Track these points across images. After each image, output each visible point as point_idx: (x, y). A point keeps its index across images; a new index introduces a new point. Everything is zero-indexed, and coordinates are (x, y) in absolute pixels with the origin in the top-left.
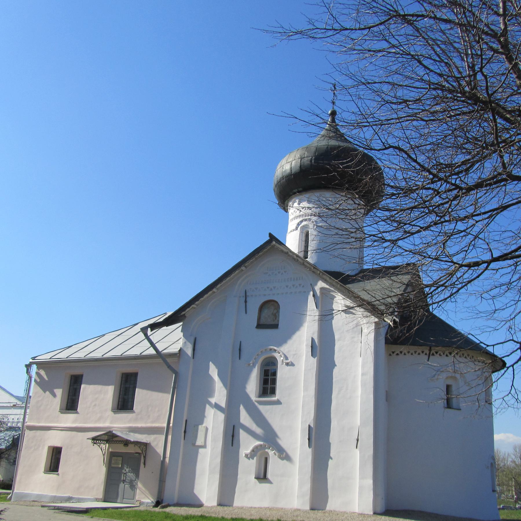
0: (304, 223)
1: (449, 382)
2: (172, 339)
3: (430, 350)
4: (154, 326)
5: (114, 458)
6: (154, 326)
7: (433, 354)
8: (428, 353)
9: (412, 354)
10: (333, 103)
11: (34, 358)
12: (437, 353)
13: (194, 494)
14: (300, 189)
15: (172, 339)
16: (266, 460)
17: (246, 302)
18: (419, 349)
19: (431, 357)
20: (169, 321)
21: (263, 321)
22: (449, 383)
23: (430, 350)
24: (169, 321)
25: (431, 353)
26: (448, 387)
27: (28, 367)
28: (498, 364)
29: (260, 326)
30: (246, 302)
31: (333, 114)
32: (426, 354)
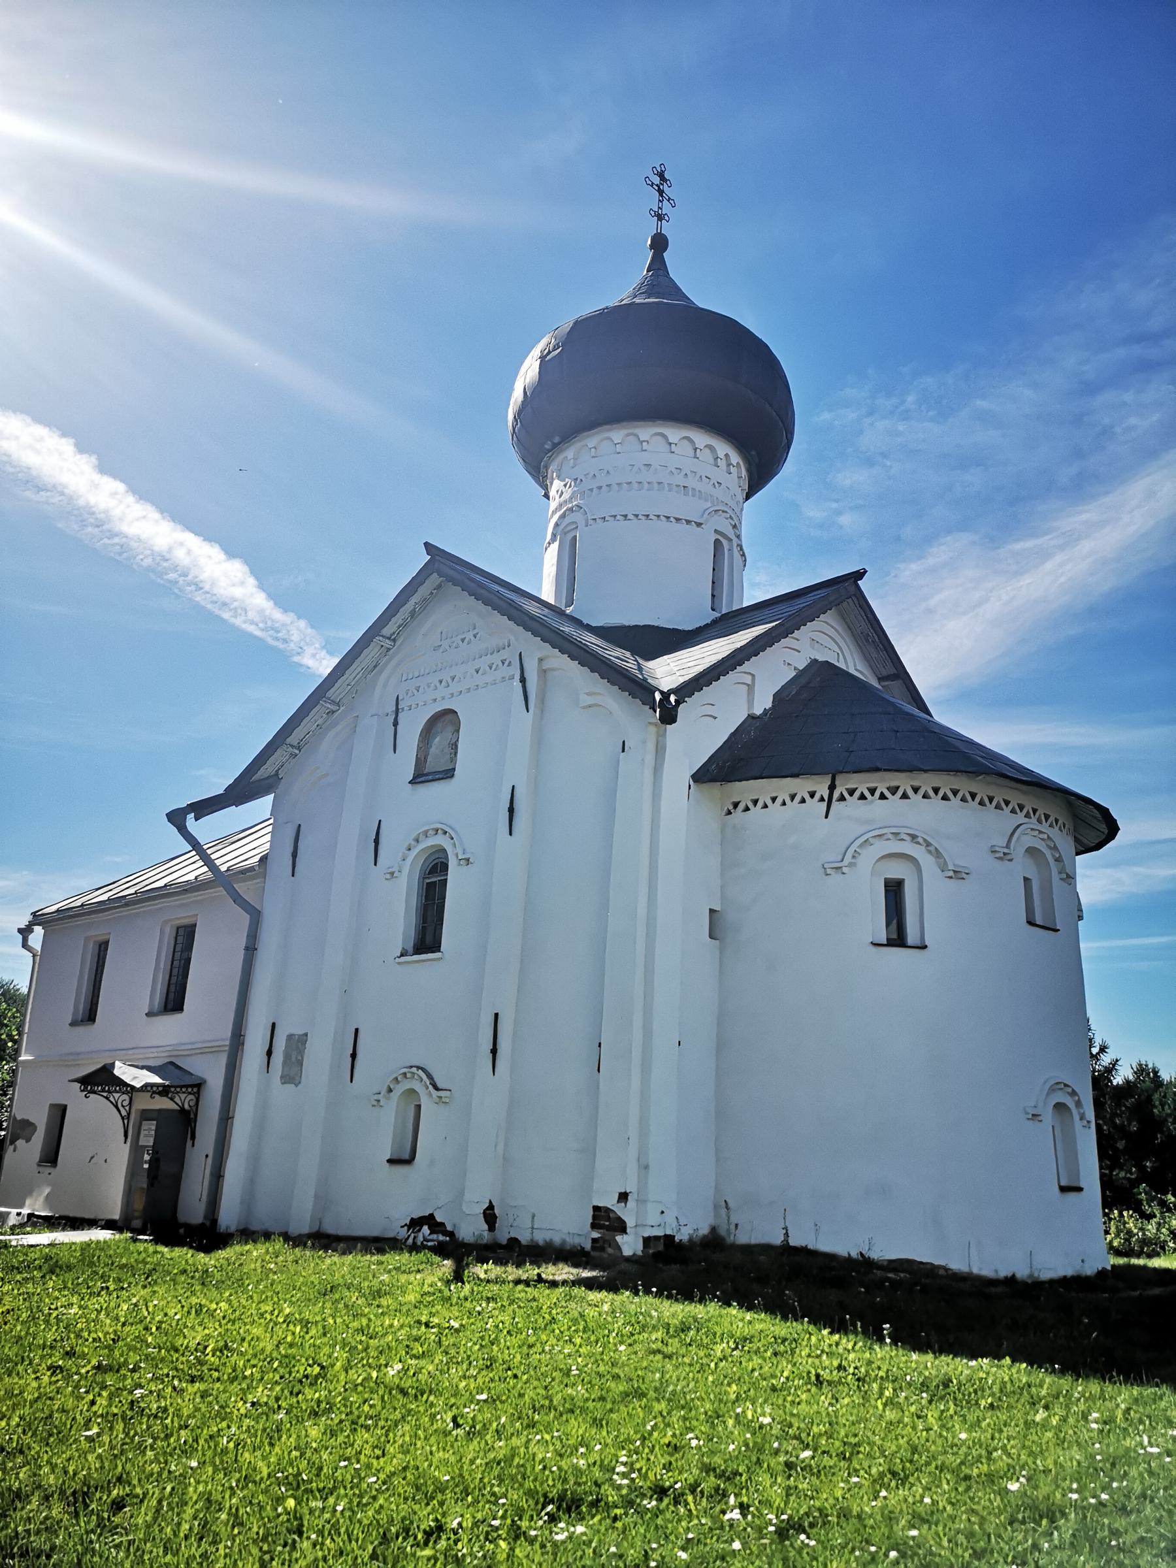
0: (567, 520)
1: (895, 871)
2: (245, 837)
3: (832, 788)
4: (203, 808)
5: (406, 1156)
6: (203, 808)
7: (842, 798)
8: (826, 798)
9: (784, 804)
10: (660, 217)
11: (34, 914)
12: (851, 792)
13: (748, 1249)
14: (557, 439)
15: (245, 837)
16: (419, 1107)
17: (396, 724)
18: (800, 786)
19: (835, 805)
20: (241, 791)
21: (431, 766)
22: (894, 875)
23: (832, 788)
24: (241, 791)
25: (836, 795)
26: (894, 890)
27: (25, 932)
28: (1093, 826)
29: (421, 777)
30: (396, 724)
31: (659, 244)
32: (822, 799)
